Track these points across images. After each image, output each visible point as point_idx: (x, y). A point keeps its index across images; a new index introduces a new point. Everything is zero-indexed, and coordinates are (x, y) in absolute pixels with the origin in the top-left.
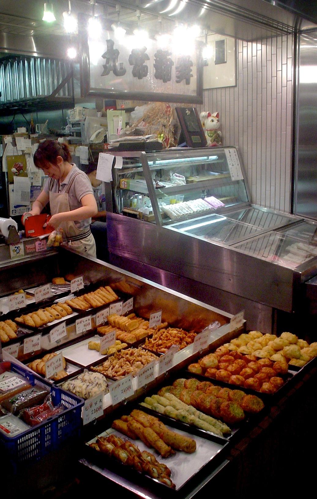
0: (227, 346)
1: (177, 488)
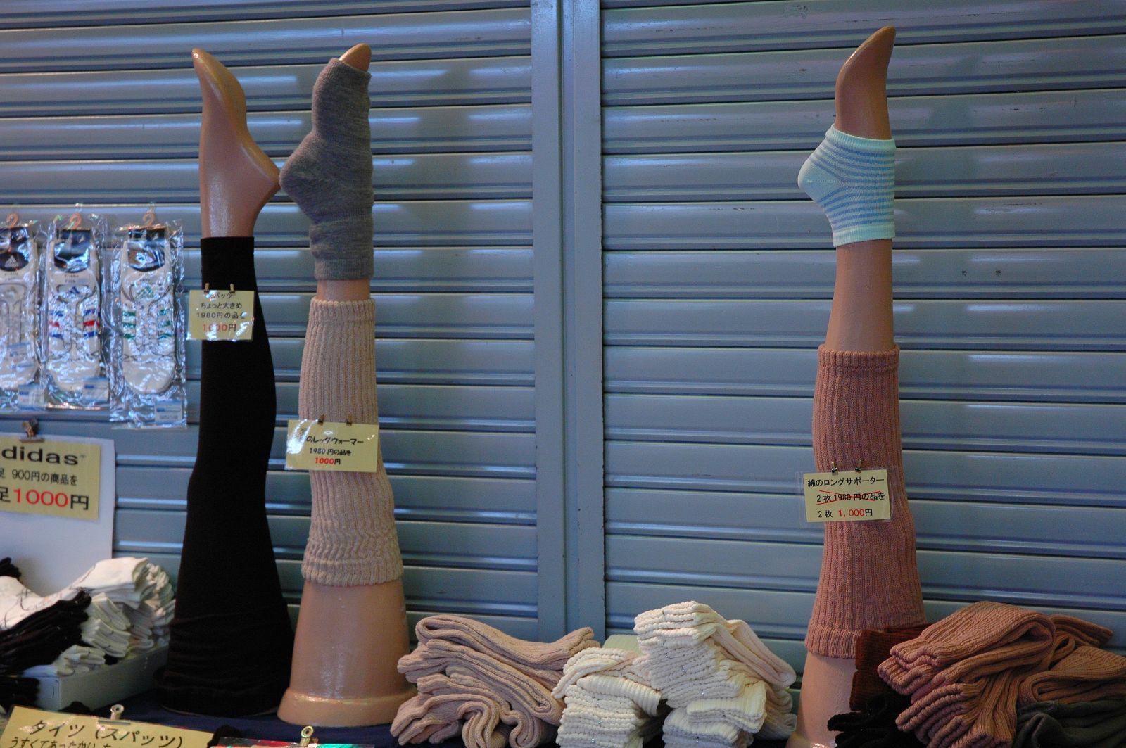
0: (487, 739)
1: (838, 733)
